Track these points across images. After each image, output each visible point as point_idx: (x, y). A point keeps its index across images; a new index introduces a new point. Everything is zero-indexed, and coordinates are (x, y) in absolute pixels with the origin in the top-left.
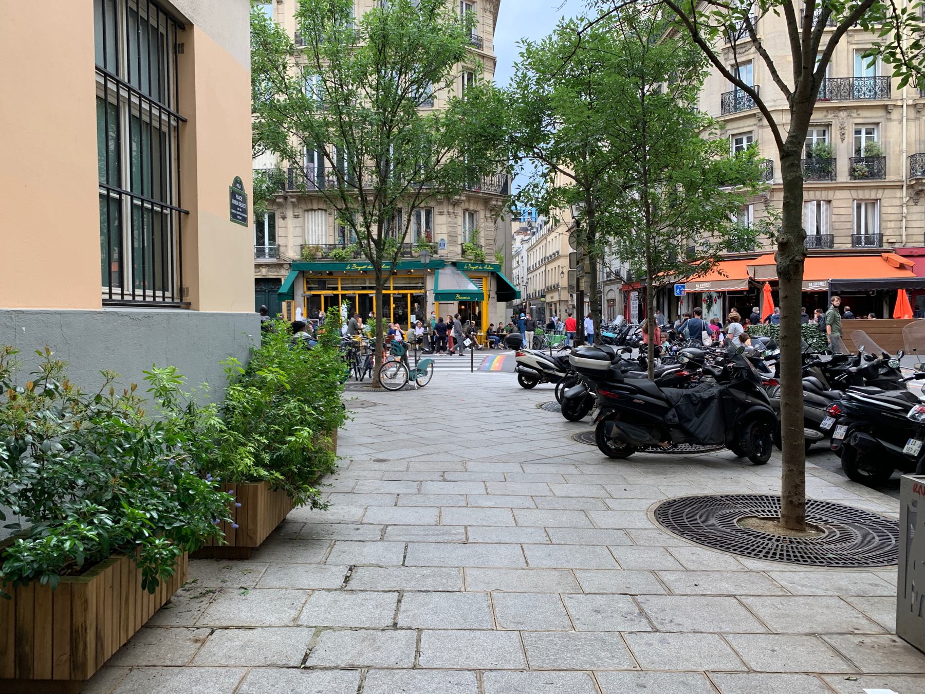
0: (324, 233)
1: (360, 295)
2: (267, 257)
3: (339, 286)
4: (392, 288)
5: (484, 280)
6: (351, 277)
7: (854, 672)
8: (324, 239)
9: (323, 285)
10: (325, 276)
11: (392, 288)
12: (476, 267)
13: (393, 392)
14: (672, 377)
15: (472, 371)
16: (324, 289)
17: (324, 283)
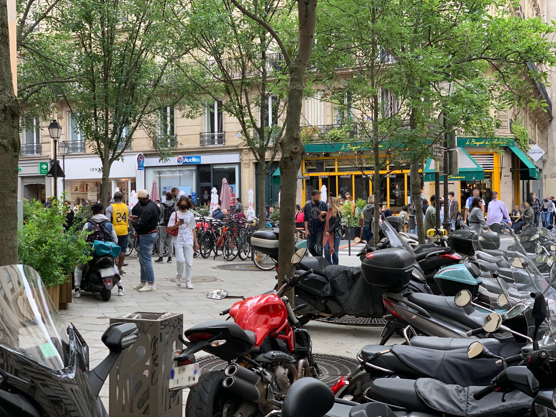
0: (322, 114)
1: (357, 177)
2: (216, 143)
3: (336, 167)
4: (336, 170)
5: (495, 156)
6: (344, 158)
7: (48, 405)
8: (322, 120)
9: (320, 167)
10: (322, 158)
11: (336, 170)
12: (482, 143)
13: (266, 272)
14: (435, 258)
15: (350, 255)
16: (322, 171)
17: (322, 164)
